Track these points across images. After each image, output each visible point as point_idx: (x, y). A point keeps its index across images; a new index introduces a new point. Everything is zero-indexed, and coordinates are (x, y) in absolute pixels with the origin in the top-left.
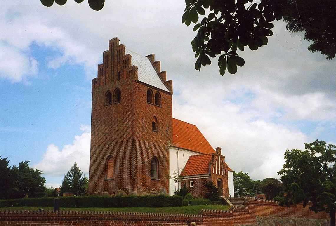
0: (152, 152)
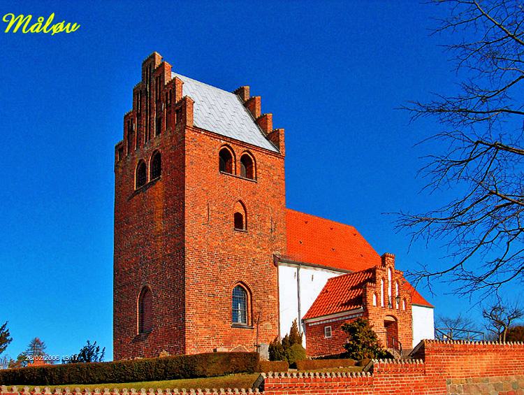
0: (234, 274)
